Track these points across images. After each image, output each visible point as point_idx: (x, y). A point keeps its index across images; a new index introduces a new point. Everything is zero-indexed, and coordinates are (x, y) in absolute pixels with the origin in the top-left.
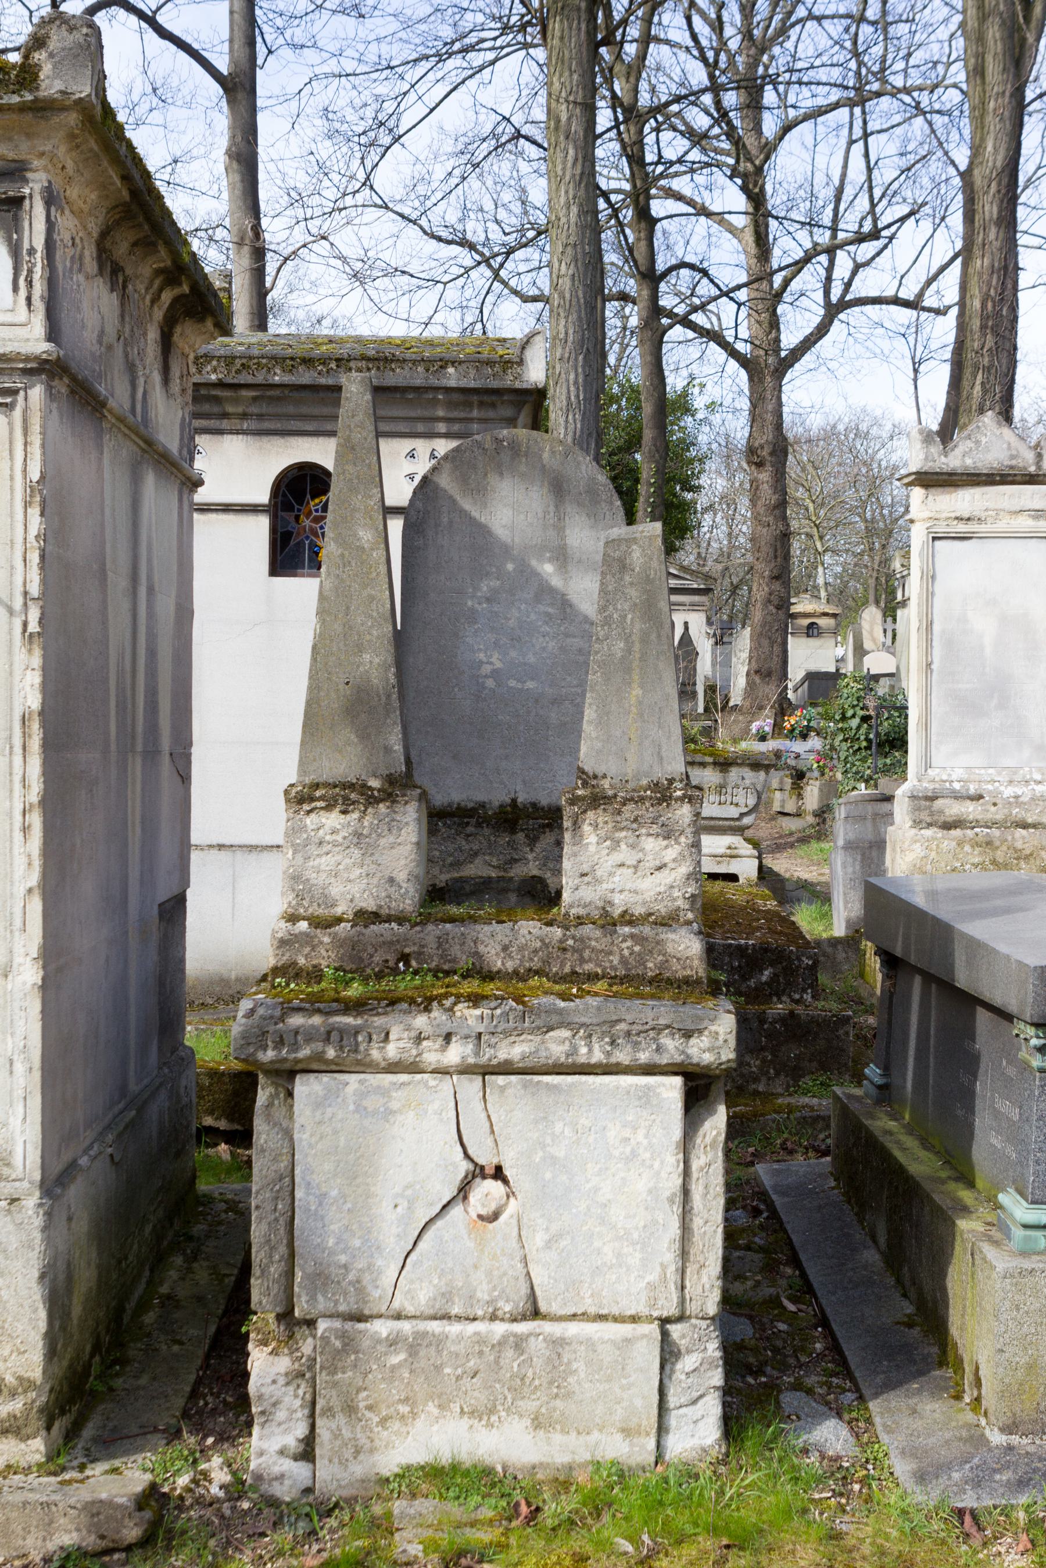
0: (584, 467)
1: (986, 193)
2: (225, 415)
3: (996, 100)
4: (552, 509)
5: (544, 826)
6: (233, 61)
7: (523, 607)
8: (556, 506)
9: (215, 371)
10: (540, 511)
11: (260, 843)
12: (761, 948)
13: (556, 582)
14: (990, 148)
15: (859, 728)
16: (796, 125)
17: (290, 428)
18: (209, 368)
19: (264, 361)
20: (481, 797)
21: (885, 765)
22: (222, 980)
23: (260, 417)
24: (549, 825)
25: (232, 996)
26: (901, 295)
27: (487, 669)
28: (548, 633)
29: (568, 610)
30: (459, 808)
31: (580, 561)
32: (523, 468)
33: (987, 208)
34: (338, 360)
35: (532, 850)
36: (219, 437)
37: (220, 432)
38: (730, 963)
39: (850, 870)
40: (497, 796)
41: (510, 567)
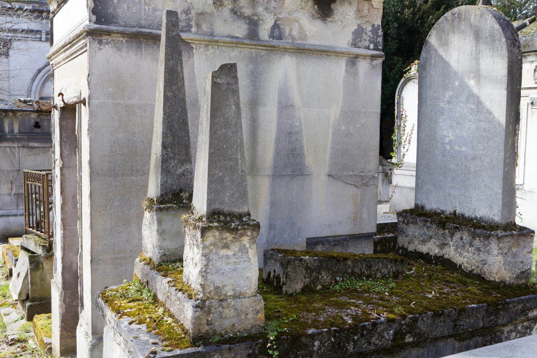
7: (462, 105)
13: (475, 90)
20: (443, 208)
27: (447, 140)
41: (457, 83)
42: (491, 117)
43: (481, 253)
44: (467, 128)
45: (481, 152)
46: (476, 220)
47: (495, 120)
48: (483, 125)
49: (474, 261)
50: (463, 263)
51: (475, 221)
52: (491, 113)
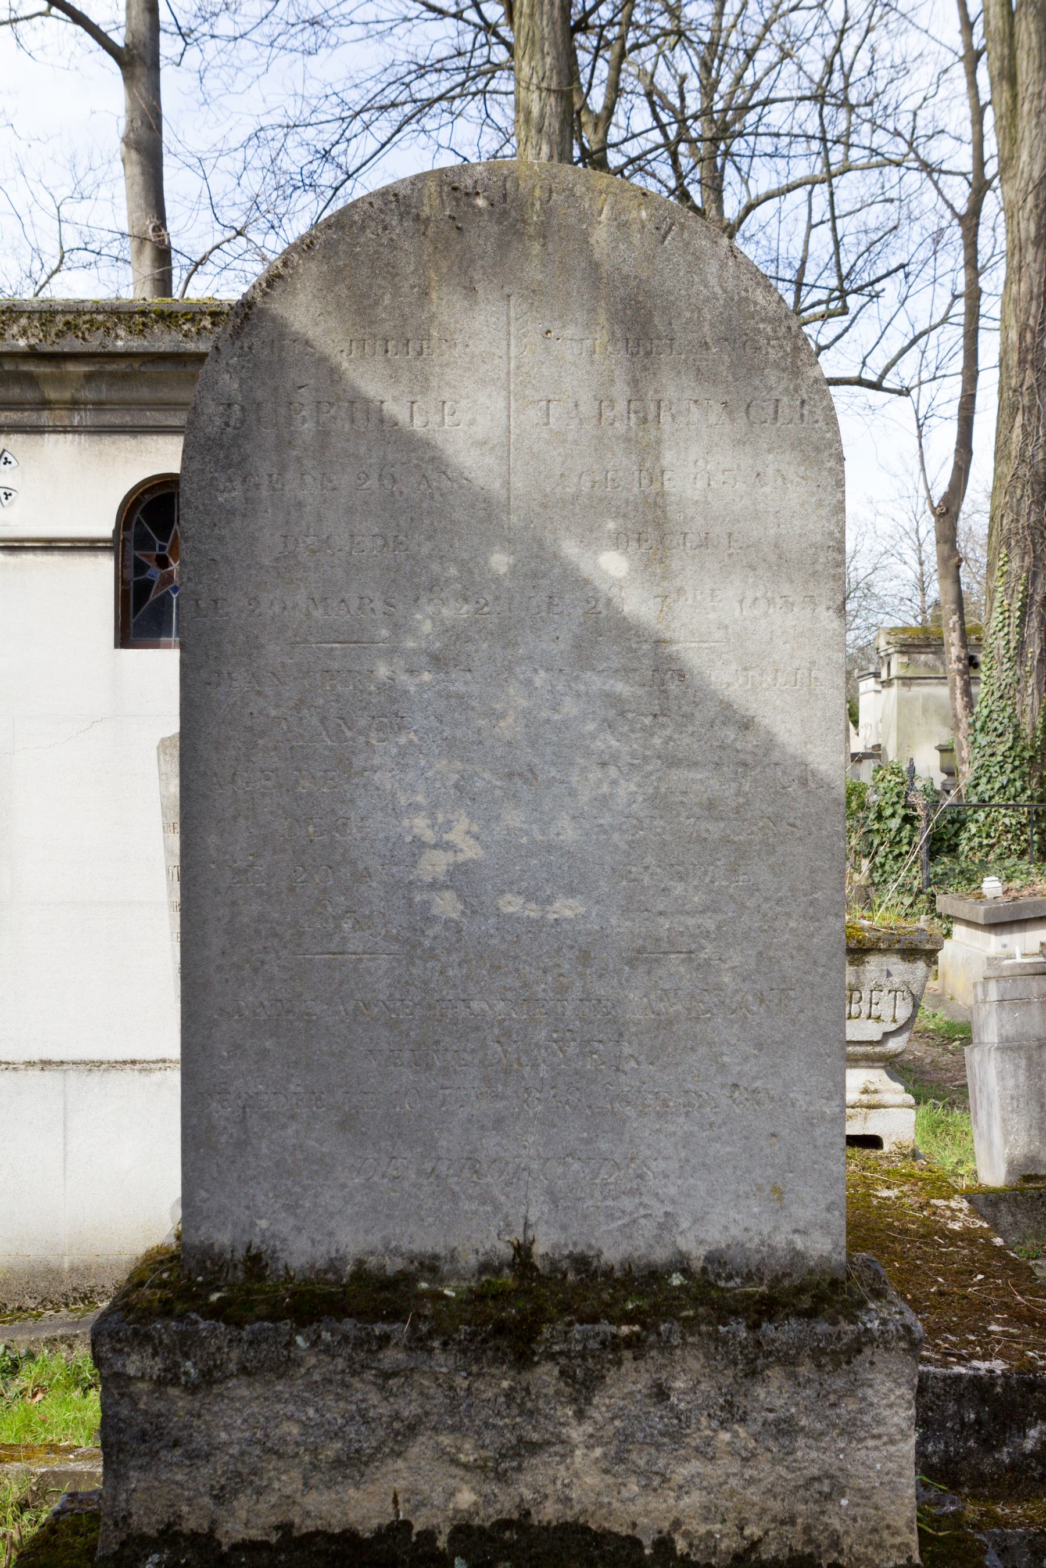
0: (713, 268)
1: (1022, 208)
2: (45, 404)
3: (1032, 102)
4: (621, 390)
5: (614, 1344)
6: (131, 32)
7: (540, 679)
8: (634, 382)
9: (24, 333)
10: (586, 397)
11: (104, 1058)
12: (1022, 1382)
13: (637, 604)
14: (1025, 157)
15: (899, 830)
16: (759, 204)
17: (144, 422)
18: (15, 329)
19: (100, 317)
20: (424, 1240)
21: (936, 875)
22: (50, 1271)
23: (99, 405)
24: (634, 1343)
25: (65, 1295)
26: (863, 376)
27: (435, 864)
28: (615, 758)
29: (673, 687)
30: (361, 1274)
31: (705, 543)
32: (533, 272)
33: (1022, 226)
34: (213, 314)
35: (580, 1415)
36: (38, 437)
37: (38, 430)
38: (959, 1416)
39: (1010, 1083)
40: (470, 1237)
41: (500, 562)
42: (750, 742)
43: (801, 1442)
44: (584, 798)
45: (691, 922)
46: (685, 1271)
47: (776, 756)
48: (700, 782)
49: (752, 1494)
50: (677, 1524)
51: (677, 1280)
52: (746, 725)
